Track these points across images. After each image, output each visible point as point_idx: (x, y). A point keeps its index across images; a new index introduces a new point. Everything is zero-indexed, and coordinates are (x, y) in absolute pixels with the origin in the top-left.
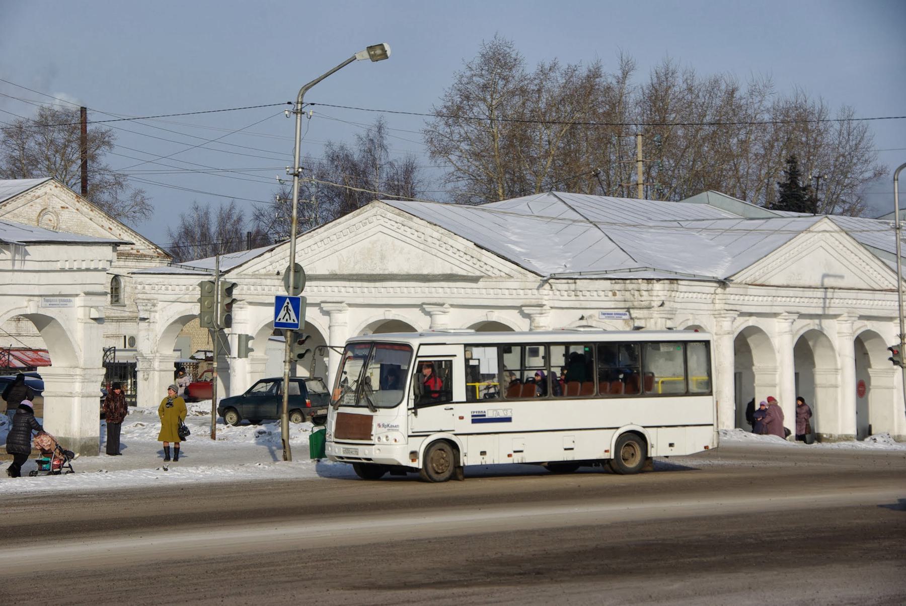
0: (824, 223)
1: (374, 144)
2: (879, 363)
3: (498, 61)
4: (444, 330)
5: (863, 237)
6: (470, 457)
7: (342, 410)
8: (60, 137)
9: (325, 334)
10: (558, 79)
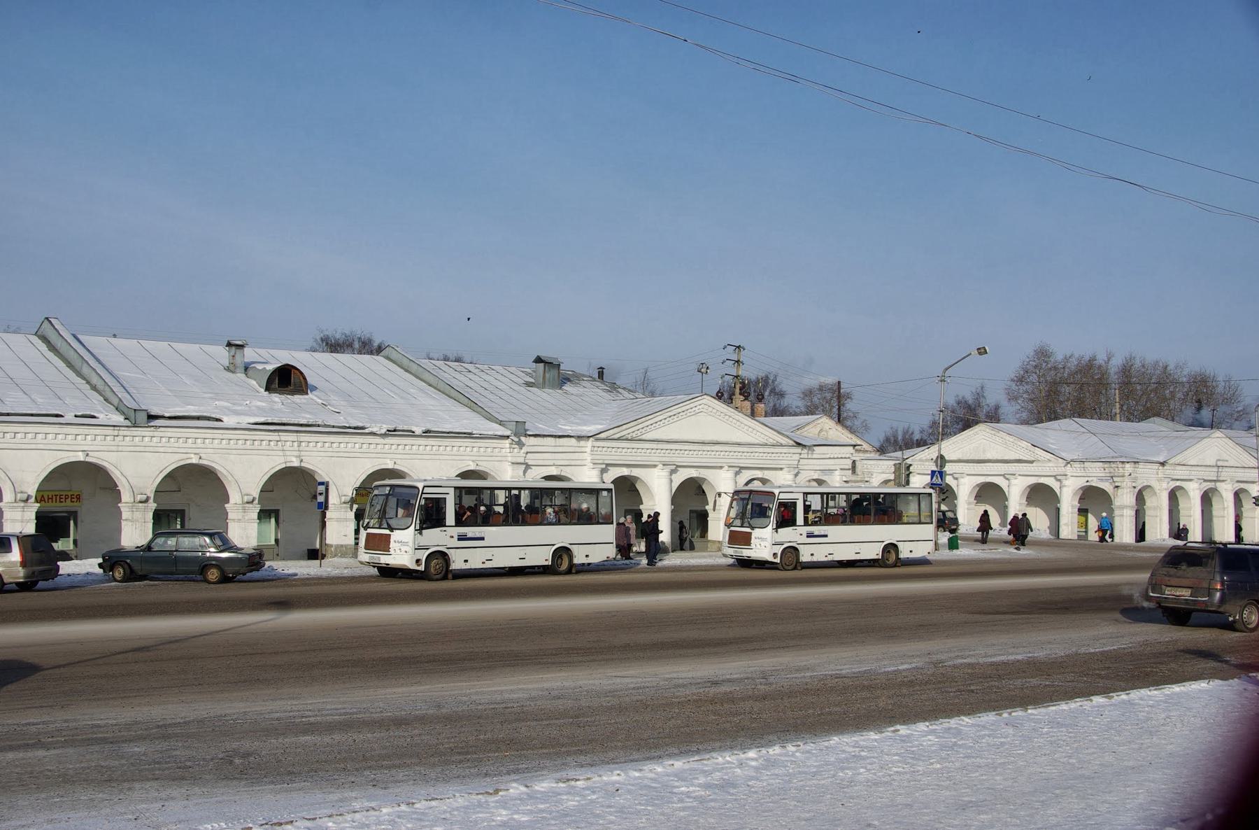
0: (1217, 433)
1: (979, 395)
2: (1247, 505)
3: (1043, 354)
4: (785, 482)
5: (1238, 440)
6: (457, 564)
7: (370, 531)
8: (828, 395)
9: (1006, 490)
10: (1074, 362)
